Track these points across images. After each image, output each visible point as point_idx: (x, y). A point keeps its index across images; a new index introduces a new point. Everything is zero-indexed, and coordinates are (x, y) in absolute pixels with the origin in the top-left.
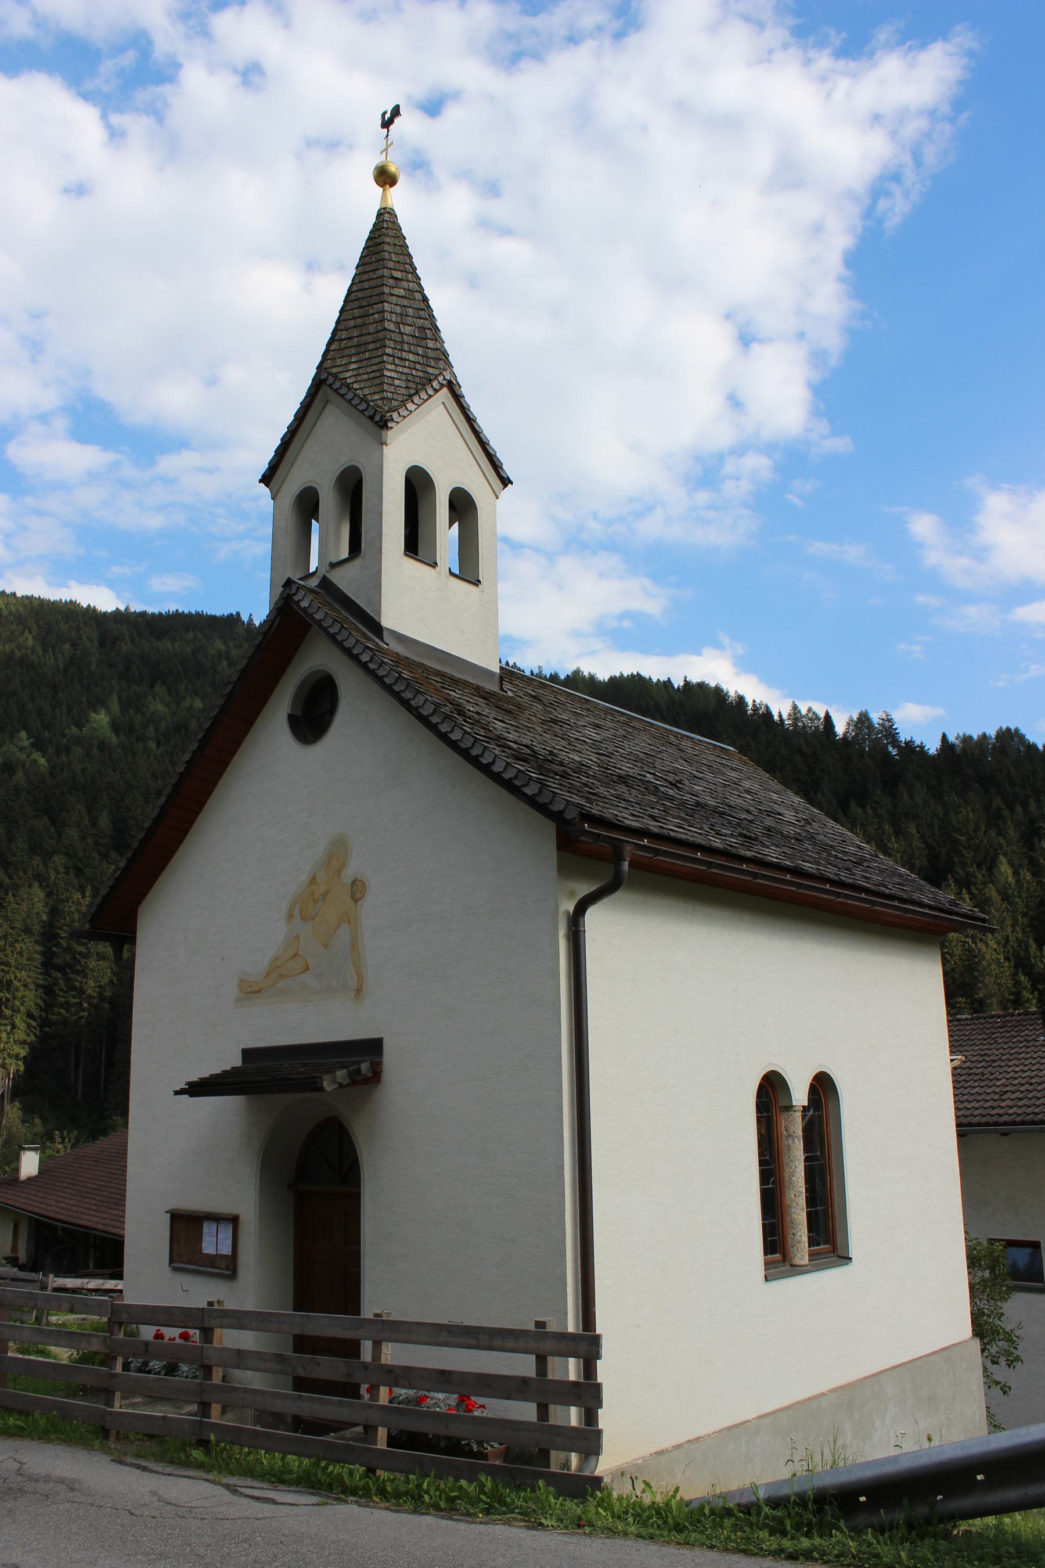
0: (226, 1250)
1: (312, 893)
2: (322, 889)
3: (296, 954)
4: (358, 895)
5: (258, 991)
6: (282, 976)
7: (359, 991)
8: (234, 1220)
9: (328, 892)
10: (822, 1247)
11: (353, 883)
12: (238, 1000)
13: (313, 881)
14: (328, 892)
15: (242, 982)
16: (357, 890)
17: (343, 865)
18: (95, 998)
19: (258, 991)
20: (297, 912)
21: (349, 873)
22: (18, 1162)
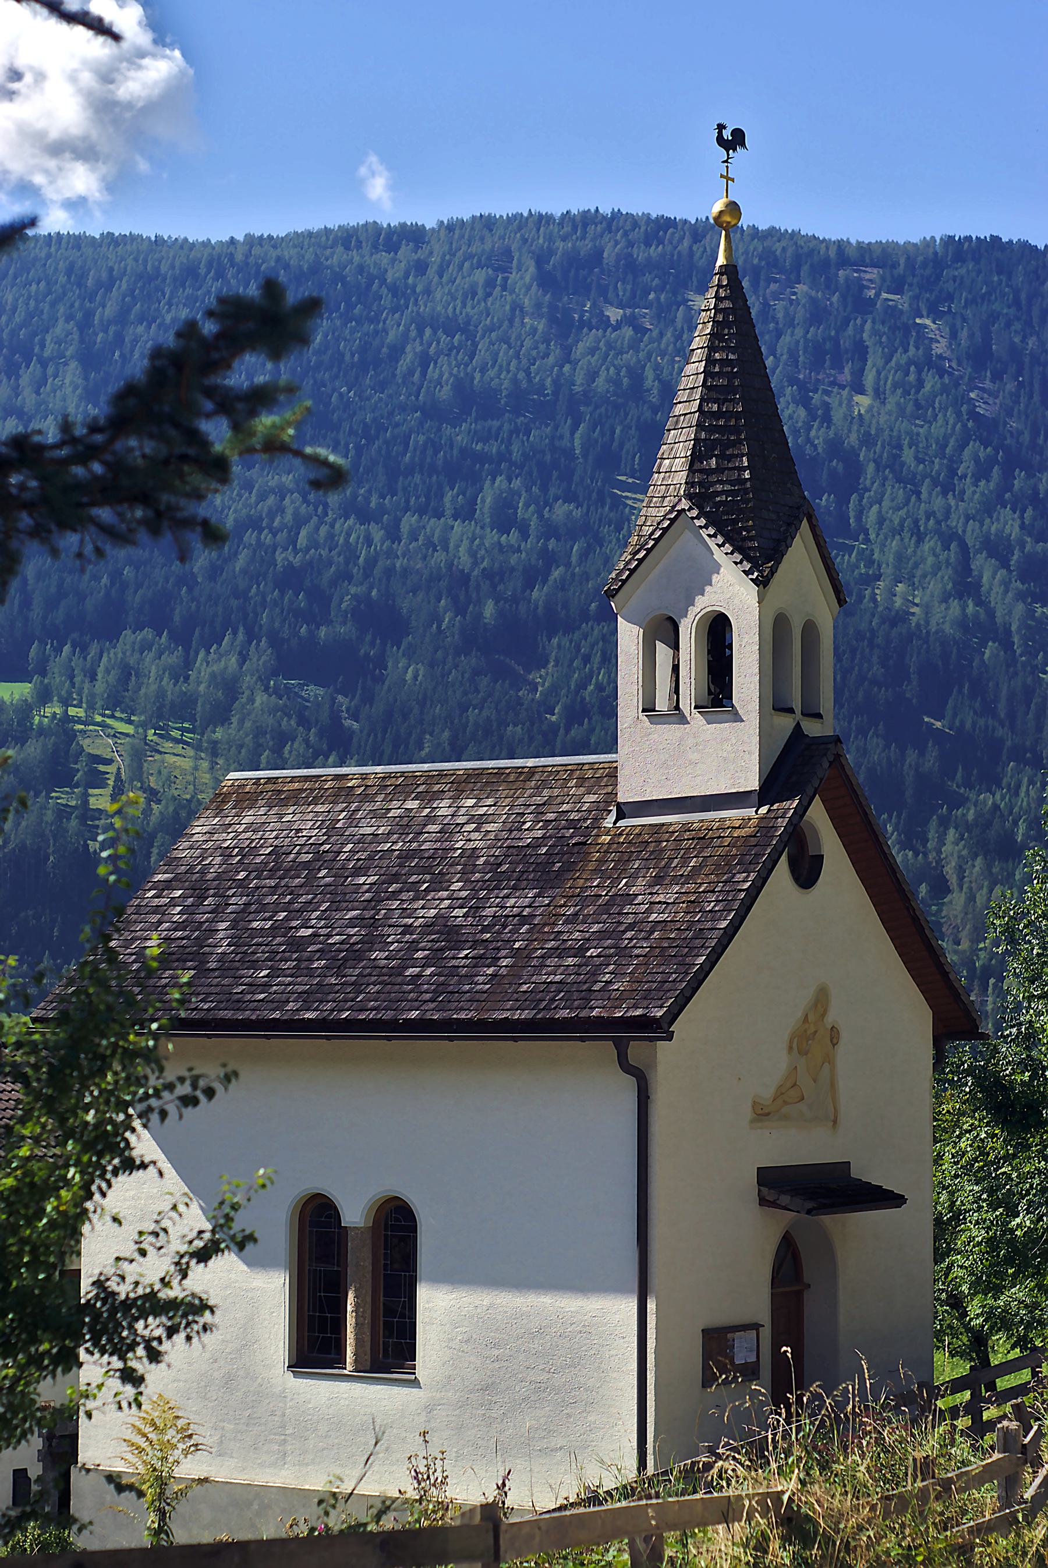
0: (754, 1359)
1: (805, 1031)
2: (812, 1029)
3: (795, 1084)
4: (835, 1041)
5: (768, 1114)
6: (785, 1103)
7: (835, 1122)
8: (756, 1327)
9: (816, 1032)
10: (382, 1299)
11: (833, 1027)
12: (752, 1121)
13: (806, 1019)
14: (816, 1032)
15: (755, 1104)
16: (834, 1036)
17: (823, 1015)
18: (245, 288)
19: (768, 1114)
20: (795, 1045)
21: (830, 1019)
22: (339, 1334)
